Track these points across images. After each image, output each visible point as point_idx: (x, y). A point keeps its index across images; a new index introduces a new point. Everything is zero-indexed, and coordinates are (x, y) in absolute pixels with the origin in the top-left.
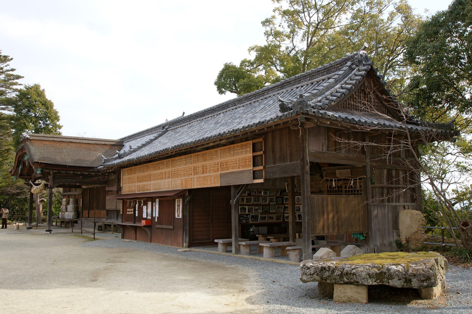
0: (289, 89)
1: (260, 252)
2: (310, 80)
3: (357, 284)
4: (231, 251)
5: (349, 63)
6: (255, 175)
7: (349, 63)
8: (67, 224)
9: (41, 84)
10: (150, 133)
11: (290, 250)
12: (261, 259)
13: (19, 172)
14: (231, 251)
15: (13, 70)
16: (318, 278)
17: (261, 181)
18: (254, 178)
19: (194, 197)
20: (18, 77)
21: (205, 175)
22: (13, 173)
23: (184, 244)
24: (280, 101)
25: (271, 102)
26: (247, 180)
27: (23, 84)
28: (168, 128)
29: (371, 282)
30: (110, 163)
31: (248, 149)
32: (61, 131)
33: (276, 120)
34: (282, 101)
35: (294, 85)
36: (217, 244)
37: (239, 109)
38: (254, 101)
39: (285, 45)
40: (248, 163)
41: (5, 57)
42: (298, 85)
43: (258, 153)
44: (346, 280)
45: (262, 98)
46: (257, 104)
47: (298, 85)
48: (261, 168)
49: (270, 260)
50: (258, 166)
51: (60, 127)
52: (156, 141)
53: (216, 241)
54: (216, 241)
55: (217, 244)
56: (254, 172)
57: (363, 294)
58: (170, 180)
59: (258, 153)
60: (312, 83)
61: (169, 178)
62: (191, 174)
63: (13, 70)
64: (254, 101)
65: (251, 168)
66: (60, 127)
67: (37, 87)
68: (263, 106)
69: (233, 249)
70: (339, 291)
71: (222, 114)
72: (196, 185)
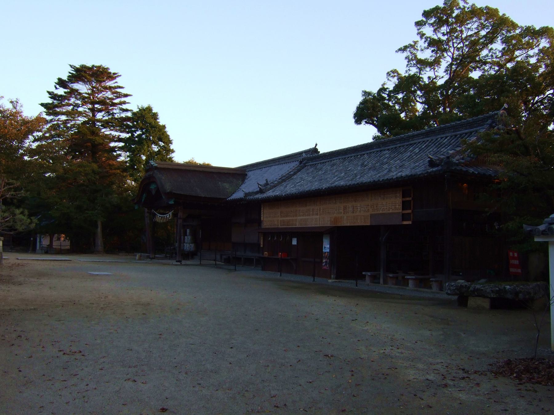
0: (434, 138)
1: (405, 282)
2: (454, 132)
3: (484, 297)
4: (379, 283)
5: (489, 121)
6: (404, 217)
7: (489, 121)
8: (188, 256)
9: (152, 106)
10: (277, 163)
11: (432, 281)
12: (408, 288)
13: (143, 200)
14: (379, 283)
15: (120, 87)
16: (458, 292)
17: (410, 223)
18: (403, 220)
19: (339, 234)
20: (126, 96)
21: (355, 214)
22: (135, 201)
23: (332, 276)
24: (429, 157)
25: (417, 150)
26: (397, 221)
27: (134, 105)
28: (306, 163)
29: (492, 295)
30: (251, 197)
31: (398, 195)
32: (173, 155)
33: (426, 175)
34: (431, 158)
35: (438, 135)
36: (365, 276)
37: (385, 152)
38: (399, 145)
39: (426, 75)
40: (397, 207)
41: (114, 74)
42: (442, 136)
43: (408, 199)
44: (476, 293)
45: (407, 143)
46: (402, 149)
47: (442, 136)
48: (410, 211)
49: (416, 289)
50: (407, 209)
51: (173, 151)
52: (295, 177)
53: (364, 273)
54: (364, 273)
55: (365, 276)
56: (403, 214)
57: (486, 303)
58: (318, 217)
59: (408, 199)
60: (456, 136)
61: (317, 214)
62: (341, 213)
63: (120, 87)
64: (399, 145)
65: (401, 211)
66: (173, 151)
67: (149, 109)
68: (409, 154)
69: (381, 281)
70: (472, 302)
71: (366, 155)
72: (346, 223)
